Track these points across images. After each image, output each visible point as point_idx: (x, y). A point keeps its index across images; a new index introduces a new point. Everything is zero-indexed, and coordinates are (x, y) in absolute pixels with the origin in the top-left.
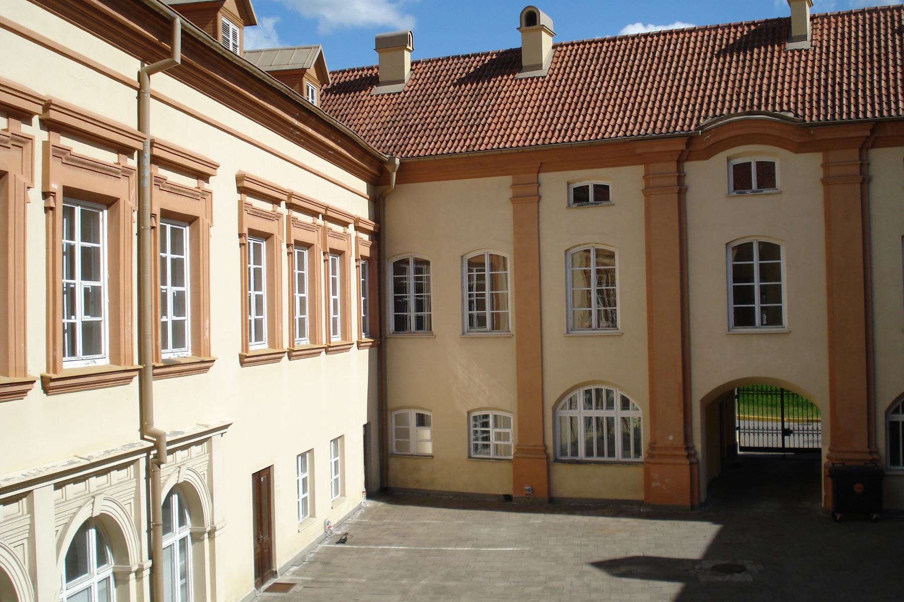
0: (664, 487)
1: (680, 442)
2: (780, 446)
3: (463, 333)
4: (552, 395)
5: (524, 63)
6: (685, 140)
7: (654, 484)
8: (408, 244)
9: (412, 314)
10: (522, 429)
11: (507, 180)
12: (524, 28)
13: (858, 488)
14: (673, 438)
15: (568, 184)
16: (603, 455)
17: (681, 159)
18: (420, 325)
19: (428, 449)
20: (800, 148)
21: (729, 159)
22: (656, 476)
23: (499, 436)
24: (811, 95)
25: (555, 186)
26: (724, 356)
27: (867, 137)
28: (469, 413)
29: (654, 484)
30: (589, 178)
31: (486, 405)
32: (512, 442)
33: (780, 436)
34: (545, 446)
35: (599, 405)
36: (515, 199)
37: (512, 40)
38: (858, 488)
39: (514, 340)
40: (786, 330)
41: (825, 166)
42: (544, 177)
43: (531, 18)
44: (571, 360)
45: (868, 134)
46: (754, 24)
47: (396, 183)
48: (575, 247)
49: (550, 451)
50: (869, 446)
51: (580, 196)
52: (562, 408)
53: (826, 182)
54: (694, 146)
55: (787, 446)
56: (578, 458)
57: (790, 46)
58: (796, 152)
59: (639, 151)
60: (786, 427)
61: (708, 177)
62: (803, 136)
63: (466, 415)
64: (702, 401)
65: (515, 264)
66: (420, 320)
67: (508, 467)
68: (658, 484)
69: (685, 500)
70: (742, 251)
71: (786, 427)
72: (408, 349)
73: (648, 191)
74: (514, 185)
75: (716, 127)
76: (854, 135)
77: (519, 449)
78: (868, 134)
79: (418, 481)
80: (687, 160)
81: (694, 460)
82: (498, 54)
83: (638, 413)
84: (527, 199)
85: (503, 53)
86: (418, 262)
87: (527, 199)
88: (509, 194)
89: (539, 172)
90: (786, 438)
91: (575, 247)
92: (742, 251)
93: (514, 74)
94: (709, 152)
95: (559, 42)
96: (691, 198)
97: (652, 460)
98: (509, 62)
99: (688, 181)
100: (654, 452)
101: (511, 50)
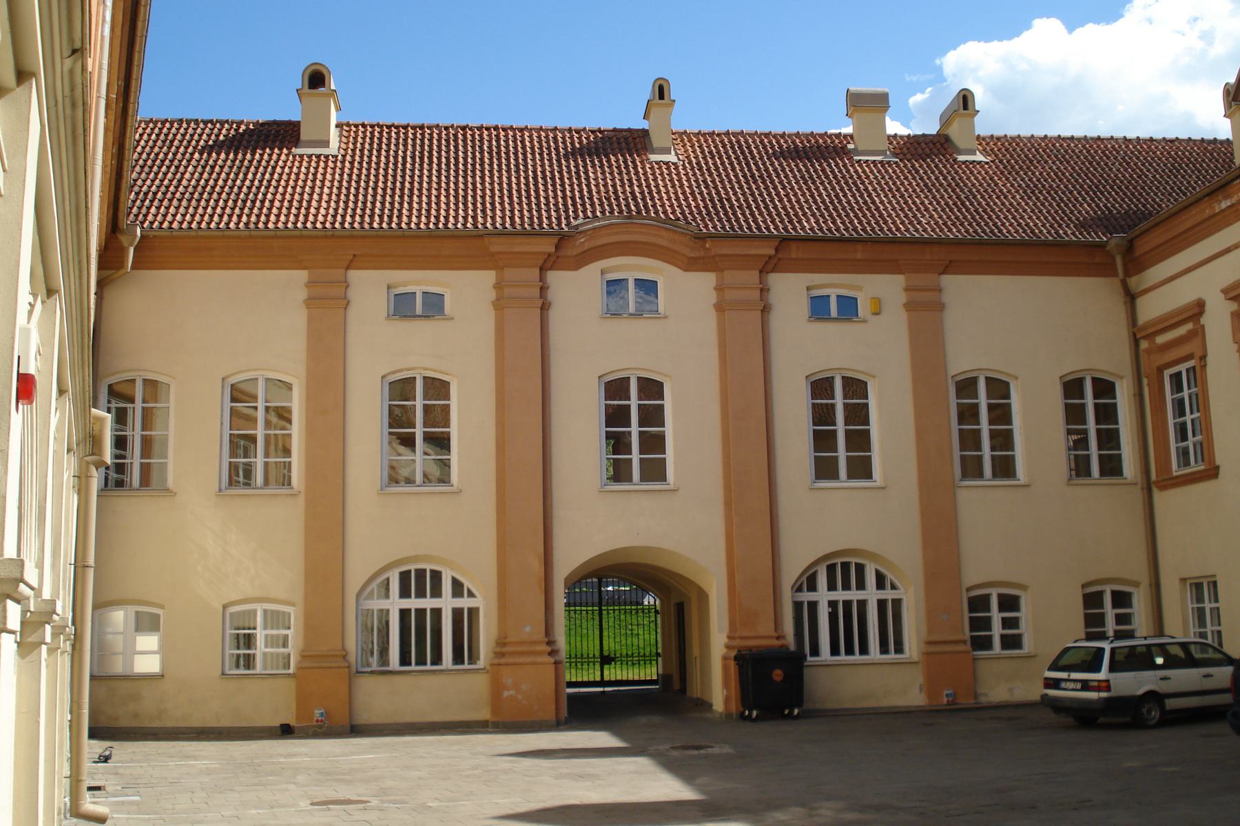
0: (520, 697)
1: (540, 635)
2: (598, 678)
3: (220, 490)
4: (357, 574)
5: (303, 137)
6: (555, 240)
7: (506, 694)
8: (136, 359)
9: (135, 460)
10: (311, 627)
11: (302, 275)
12: (306, 90)
13: (778, 675)
14: (532, 630)
15: (389, 287)
16: (425, 663)
17: (547, 264)
18: (145, 481)
19: (148, 664)
20: (691, 265)
21: (603, 272)
22: (509, 681)
23: (270, 641)
24: (697, 207)
25: (370, 289)
26: (598, 521)
27: (770, 257)
28: (225, 607)
29: (506, 694)
30: (418, 281)
31: (250, 592)
32: (293, 650)
33: (598, 666)
34: (344, 649)
35: (421, 594)
36: (311, 302)
37: (287, 109)
38: (778, 675)
39: (302, 499)
40: (671, 487)
41: (719, 289)
42: (354, 275)
43: (316, 79)
44: (387, 528)
45: (772, 252)
46: (600, 131)
47: (133, 267)
48: (394, 373)
49: (352, 658)
50: (776, 630)
51: (402, 307)
52: (366, 598)
53: (720, 308)
54: (564, 250)
55: (606, 678)
56: (390, 668)
57: (654, 158)
58: (686, 270)
59: (494, 249)
60: (606, 653)
61: (576, 291)
62: (699, 248)
63: (221, 609)
64: (566, 579)
65: (308, 388)
66: (146, 470)
67: (291, 685)
68: (512, 692)
69: (549, 714)
70: (616, 388)
71: (606, 653)
72: (134, 508)
73: (499, 305)
74: (310, 284)
75: (594, 228)
76: (753, 252)
77: (304, 656)
78: (772, 252)
79: (136, 716)
80: (551, 269)
81: (558, 659)
82: (257, 124)
83: (483, 601)
84: (328, 305)
85: (263, 124)
86: (146, 382)
87: (328, 305)
88: (302, 294)
89: (347, 268)
90: (606, 667)
91: (394, 373)
92: (616, 388)
93: (289, 149)
94: (580, 261)
95: (345, 121)
96: (554, 315)
97: (503, 660)
98: (282, 134)
99: (551, 295)
100: (504, 650)
101: (275, 122)
